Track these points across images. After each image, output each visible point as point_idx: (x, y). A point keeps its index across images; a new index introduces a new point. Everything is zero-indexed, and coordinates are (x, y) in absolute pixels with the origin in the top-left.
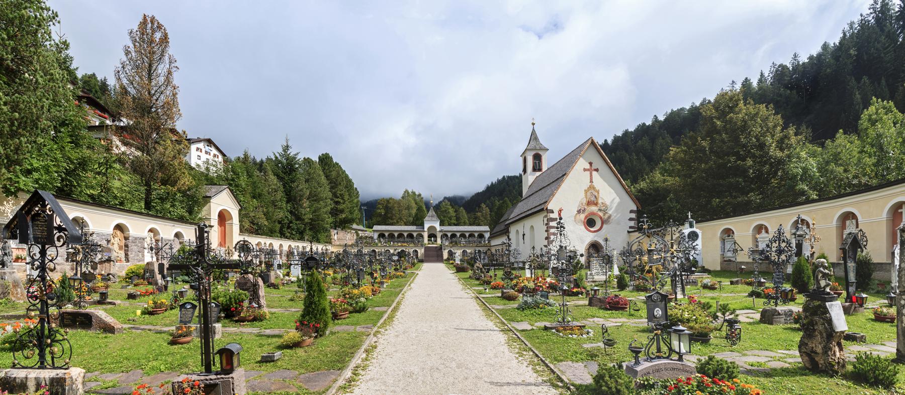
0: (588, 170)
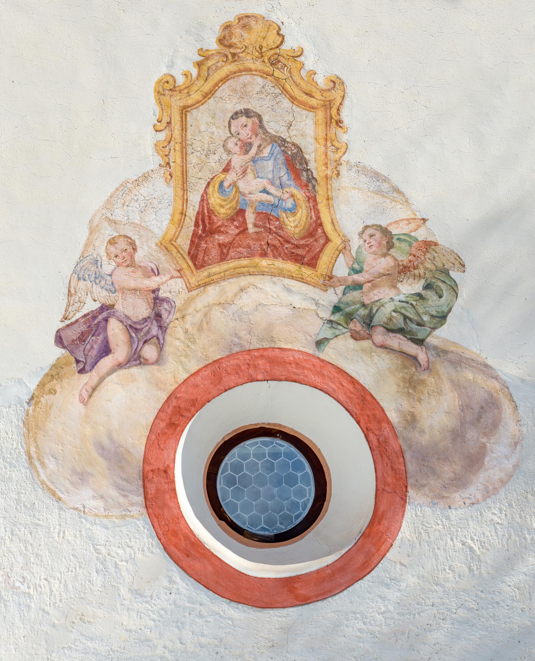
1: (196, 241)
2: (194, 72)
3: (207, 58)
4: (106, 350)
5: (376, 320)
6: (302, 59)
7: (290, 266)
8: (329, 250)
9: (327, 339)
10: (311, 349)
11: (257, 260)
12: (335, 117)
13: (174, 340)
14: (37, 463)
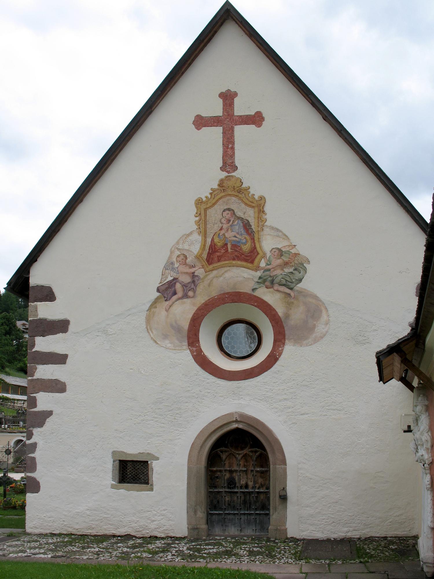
0: (214, 121)
1: (209, 254)
2: (209, 196)
3: (214, 191)
4: (175, 293)
5: (275, 282)
6: (249, 190)
7: (244, 263)
8: (259, 257)
9: (256, 288)
10: (250, 292)
11: (231, 261)
12: (262, 210)
13: (199, 290)
14: (150, 331)
